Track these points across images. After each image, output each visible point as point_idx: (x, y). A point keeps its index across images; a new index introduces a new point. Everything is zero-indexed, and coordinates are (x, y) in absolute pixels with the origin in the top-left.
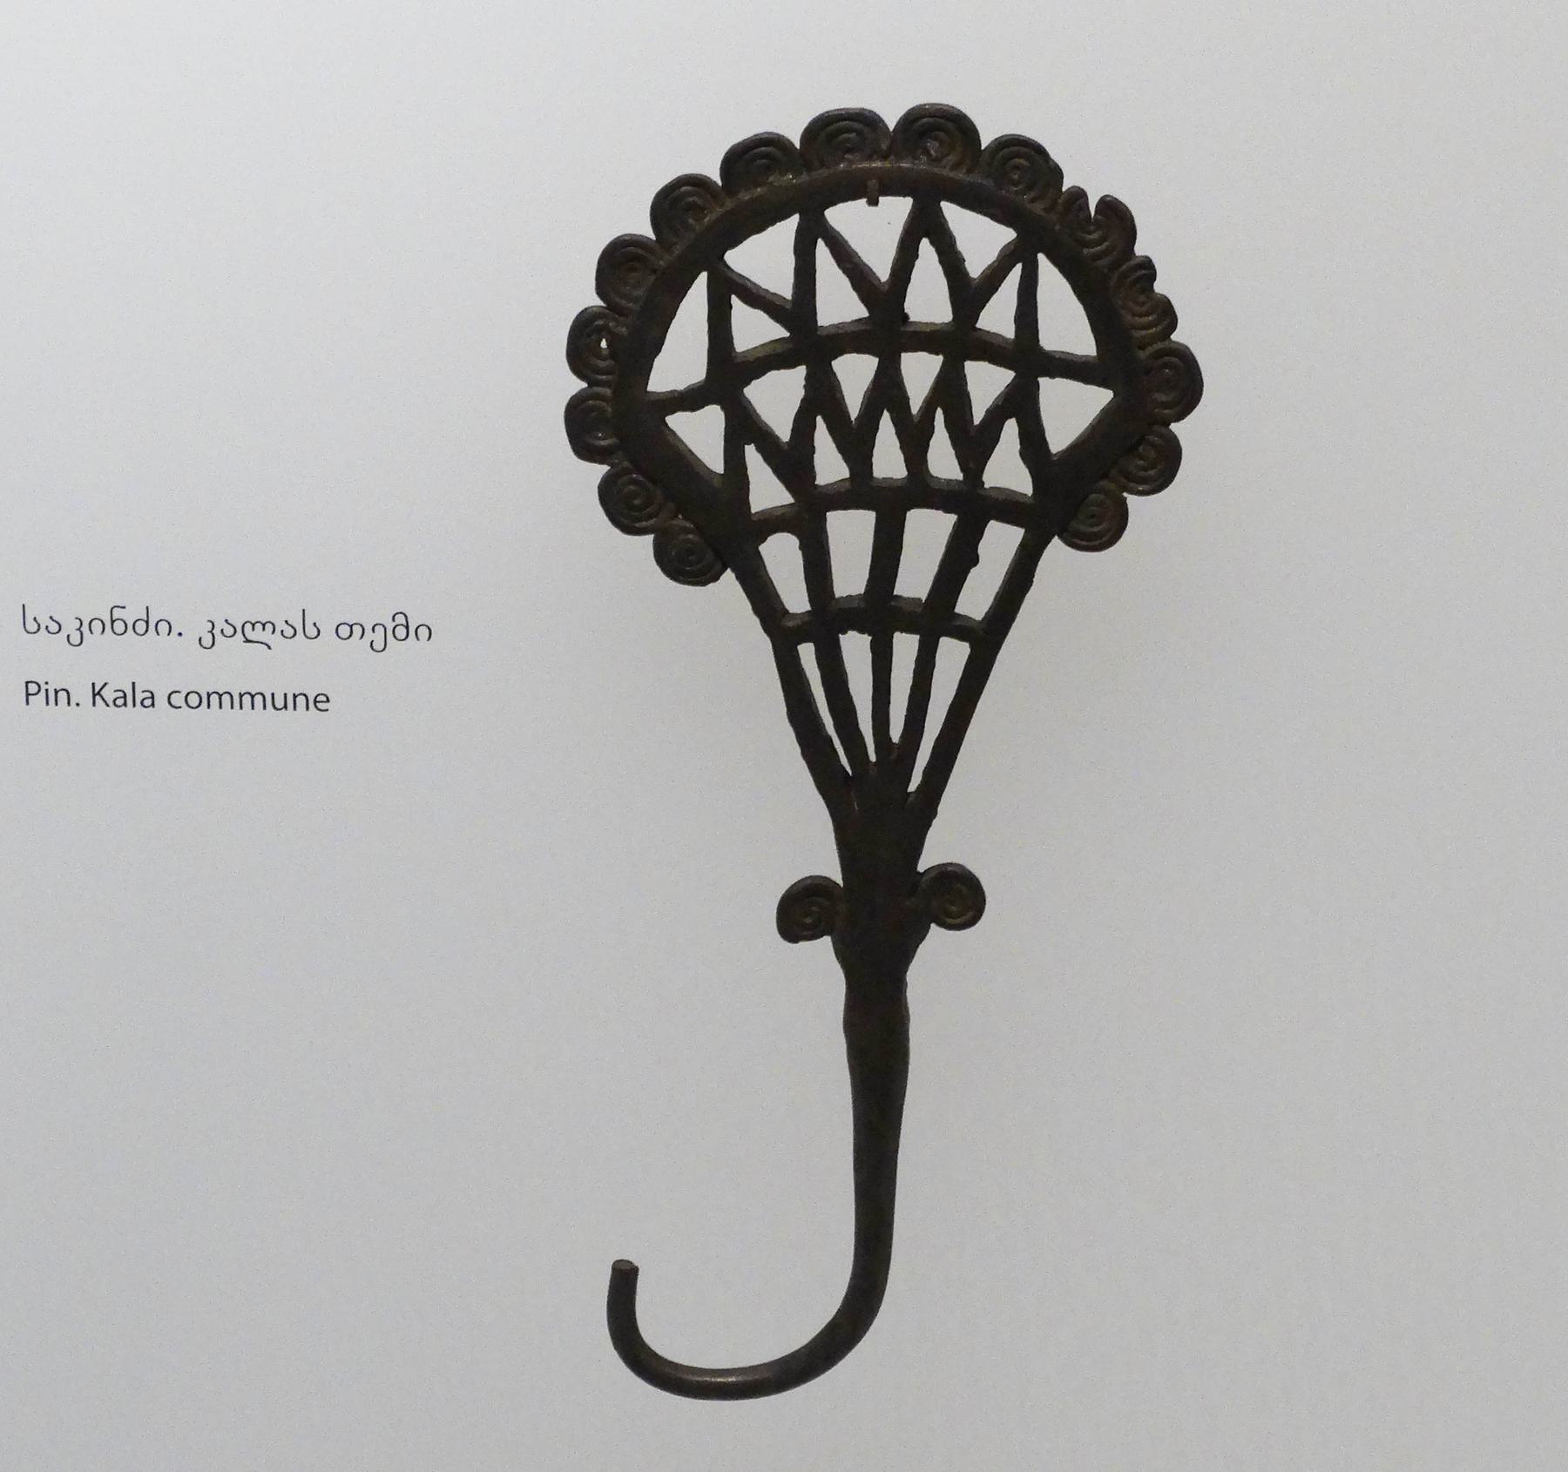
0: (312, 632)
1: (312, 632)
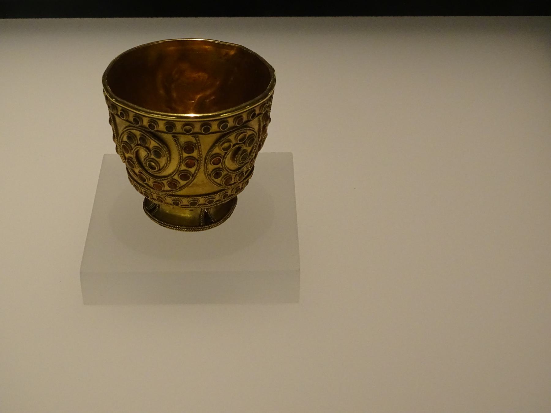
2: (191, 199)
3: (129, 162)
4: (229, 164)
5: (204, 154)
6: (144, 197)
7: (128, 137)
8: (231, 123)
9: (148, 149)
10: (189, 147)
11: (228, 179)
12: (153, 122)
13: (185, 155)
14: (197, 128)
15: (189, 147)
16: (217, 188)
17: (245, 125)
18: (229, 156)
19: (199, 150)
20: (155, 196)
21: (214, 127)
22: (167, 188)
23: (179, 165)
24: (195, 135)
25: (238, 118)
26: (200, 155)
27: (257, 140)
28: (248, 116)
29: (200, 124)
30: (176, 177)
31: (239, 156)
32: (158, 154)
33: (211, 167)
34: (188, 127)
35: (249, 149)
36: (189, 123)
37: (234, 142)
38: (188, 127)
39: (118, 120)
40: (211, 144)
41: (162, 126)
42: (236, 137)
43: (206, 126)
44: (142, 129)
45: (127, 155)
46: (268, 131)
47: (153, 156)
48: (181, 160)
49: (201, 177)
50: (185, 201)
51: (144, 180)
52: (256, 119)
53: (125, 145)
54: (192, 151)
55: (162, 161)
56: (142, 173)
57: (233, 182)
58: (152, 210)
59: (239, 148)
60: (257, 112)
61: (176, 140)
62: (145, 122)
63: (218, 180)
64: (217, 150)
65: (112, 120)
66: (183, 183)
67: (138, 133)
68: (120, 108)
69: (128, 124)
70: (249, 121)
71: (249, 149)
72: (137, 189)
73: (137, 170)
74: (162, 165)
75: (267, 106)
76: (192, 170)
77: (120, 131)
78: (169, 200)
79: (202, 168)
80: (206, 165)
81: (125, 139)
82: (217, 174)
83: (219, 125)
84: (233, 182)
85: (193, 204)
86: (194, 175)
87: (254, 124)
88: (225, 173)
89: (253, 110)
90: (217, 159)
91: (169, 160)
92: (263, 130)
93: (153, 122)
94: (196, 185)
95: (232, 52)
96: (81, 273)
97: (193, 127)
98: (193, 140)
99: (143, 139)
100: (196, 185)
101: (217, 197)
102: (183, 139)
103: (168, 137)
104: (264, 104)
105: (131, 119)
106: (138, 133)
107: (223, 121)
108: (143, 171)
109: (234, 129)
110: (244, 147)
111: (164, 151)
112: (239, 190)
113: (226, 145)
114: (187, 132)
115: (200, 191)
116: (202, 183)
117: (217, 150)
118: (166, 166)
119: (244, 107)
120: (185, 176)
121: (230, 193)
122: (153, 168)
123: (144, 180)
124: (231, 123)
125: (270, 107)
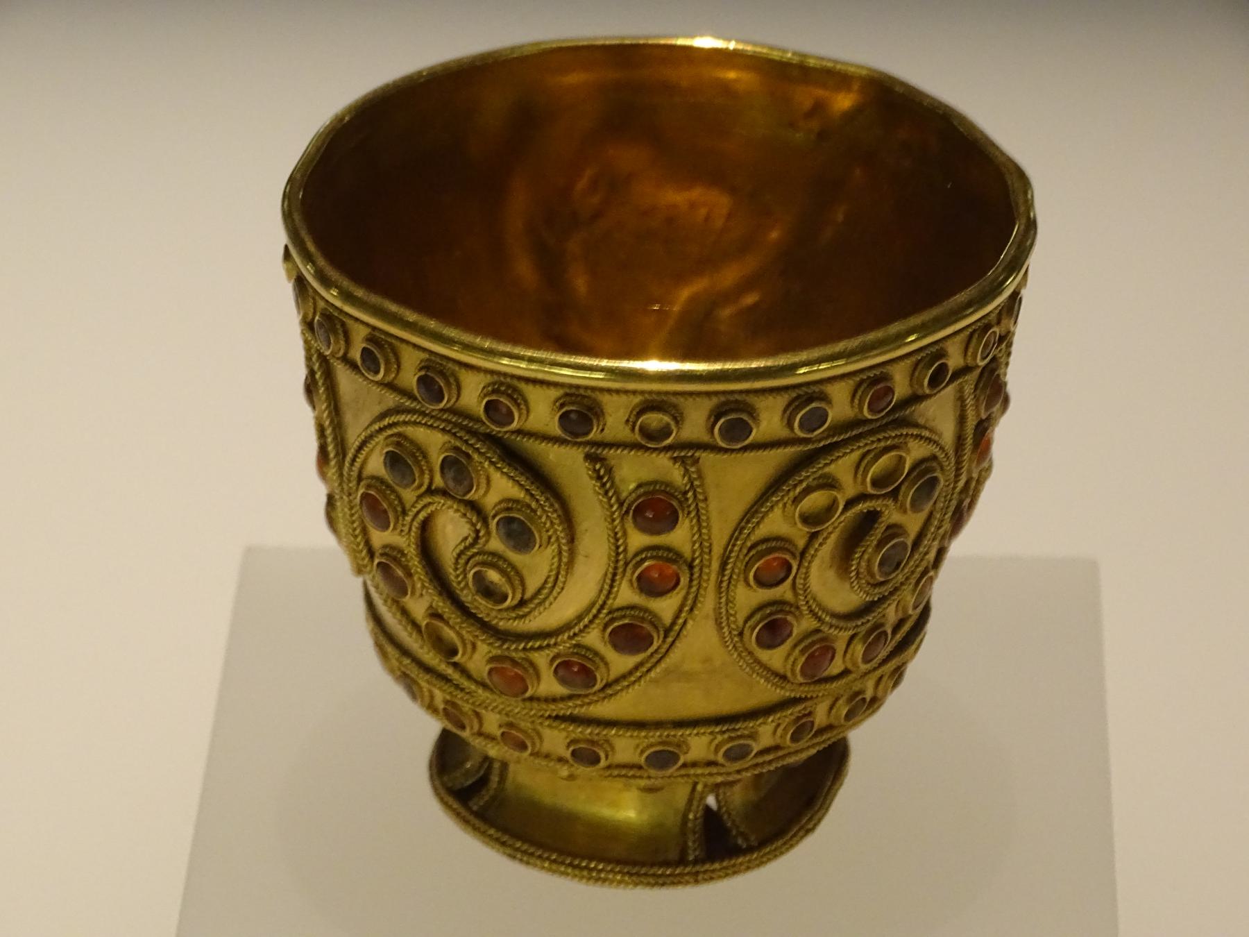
2: (655, 735)
3: (385, 568)
4: (828, 587)
5: (719, 535)
7: (393, 460)
8: (840, 406)
9: (474, 506)
10: (656, 508)
11: (818, 651)
12: (506, 393)
13: (637, 540)
14: (695, 425)
16: (766, 692)
19: (700, 521)
20: (492, 723)
21: (769, 420)
22: (549, 685)
23: (612, 580)
24: (687, 452)
25: (874, 384)
26: (704, 545)
27: (949, 486)
29: (708, 405)
30: (594, 638)
31: (869, 555)
33: (747, 597)
34: (655, 419)
36: (659, 402)
37: (850, 489)
38: (655, 419)
39: (345, 379)
40: (750, 495)
41: (542, 412)
44: (458, 422)
45: (380, 538)
47: (496, 544)
48: (619, 562)
49: (701, 640)
50: (626, 748)
52: (949, 392)
53: (367, 495)
55: (536, 565)
56: (433, 605)
57: (836, 667)
58: (469, 785)
59: (872, 517)
60: (954, 360)
62: (472, 395)
63: (775, 658)
65: (320, 384)
66: (621, 663)
67: (434, 442)
69: (391, 399)
70: (915, 399)
74: (532, 584)
75: (995, 339)
76: (665, 607)
78: (556, 739)
79: (708, 602)
81: (376, 464)
84: (836, 667)
85: (663, 759)
86: (673, 632)
87: (940, 413)
90: (777, 562)
92: (976, 440)
93: (506, 393)
95: (844, 102)
97: (678, 419)
98: (676, 475)
99: (456, 465)
101: (766, 733)
102: (633, 471)
103: (566, 462)
104: (984, 327)
105: (410, 377)
106: (434, 442)
109: (852, 430)
110: (892, 514)
111: (547, 520)
113: (816, 500)
114: (651, 439)
115: (697, 703)
116: (704, 667)
117: (776, 522)
118: (554, 584)
122: (488, 592)
124: (840, 406)
125: (1005, 339)
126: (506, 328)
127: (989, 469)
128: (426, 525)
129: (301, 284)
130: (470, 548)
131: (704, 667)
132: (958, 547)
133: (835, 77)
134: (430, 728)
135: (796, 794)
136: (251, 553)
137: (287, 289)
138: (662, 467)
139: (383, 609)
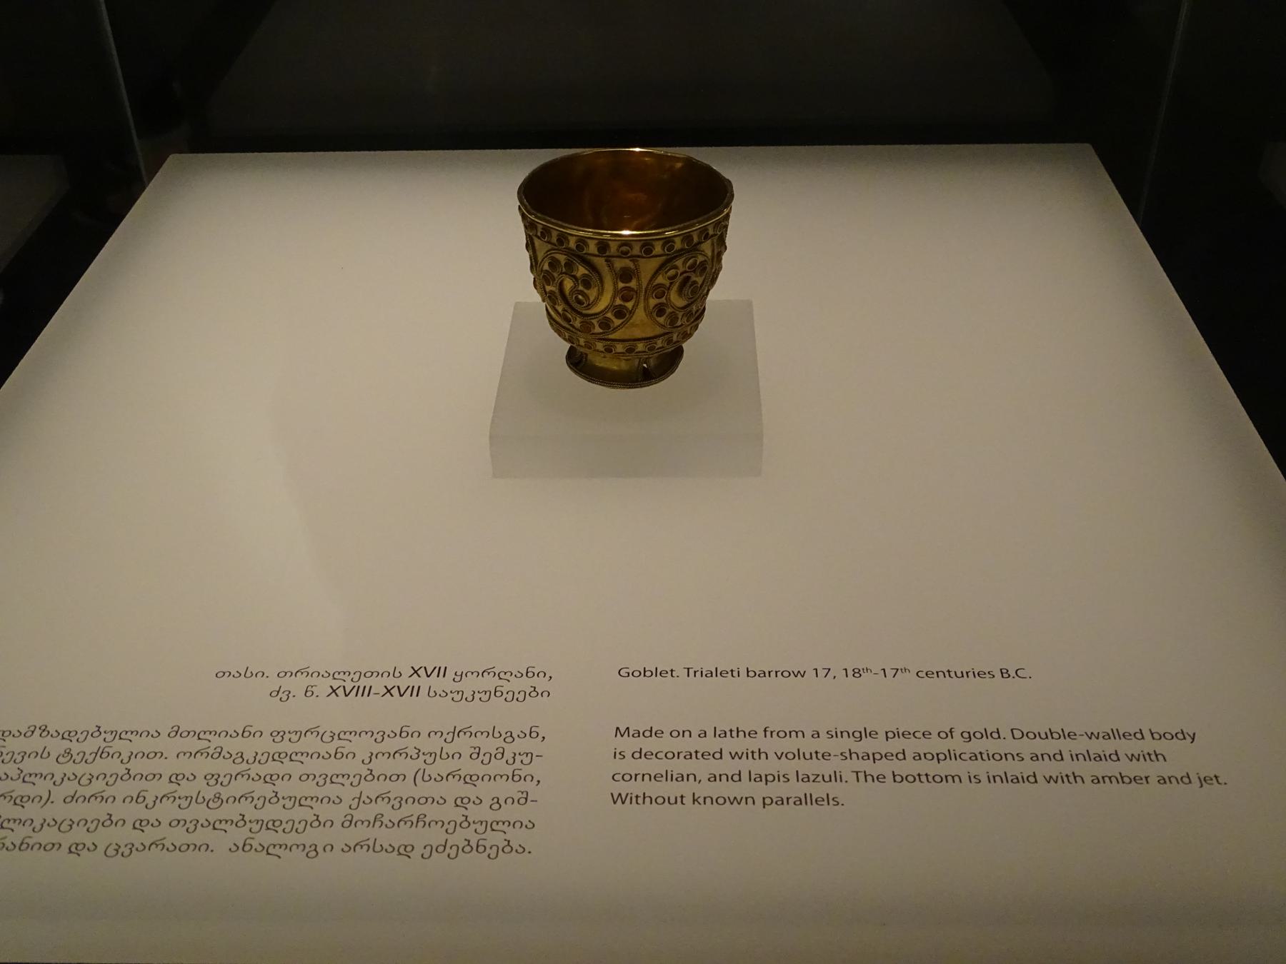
0: (397, 674)
1: (397, 674)
2: (627, 344)
3: (549, 297)
4: (677, 300)
5: (644, 283)
6: (568, 346)
7: (550, 264)
8: (678, 245)
9: (574, 277)
10: (626, 275)
11: (673, 318)
12: (582, 242)
13: (621, 285)
14: (636, 250)
15: (626, 275)
16: (659, 331)
17: (693, 248)
18: (675, 288)
19: (639, 279)
20: (582, 341)
21: (658, 249)
22: (598, 330)
23: (614, 298)
24: (634, 258)
25: (687, 238)
26: (640, 285)
27: (710, 271)
28: (699, 237)
29: (640, 244)
30: (609, 315)
31: (688, 290)
32: (587, 284)
33: (653, 302)
34: (624, 248)
35: (700, 280)
36: (626, 242)
37: (681, 269)
38: (624, 248)
39: (537, 242)
40: (652, 272)
41: (592, 248)
42: (685, 263)
43: (647, 247)
44: (569, 252)
45: (548, 288)
46: (723, 261)
47: (581, 288)
48: (616, 292)
49: (640, 314)
50: (620, 348)
51: (568, 320)
52: (709, 242)
53: (544, 276)
54: (630, 280)
55: (592, 293)
56: (566, 310)
57: (679, 323)
58: (577, 362)
59: (688, 278)
60: (711, 232)
61: (611, 265)
62: (572, 244)
63: (661, 320)
64: (660, 279)
65: (530, 245)
66: (617, 322)
67: (562, 258)
68: (540, 227)
69: (550, 246)
70: (700, 243)
71: (700, 280)
72: (557, 331)
73: (560, 309)
74: (592, 299)
75: (722, 226)
76: (629, 305)
77: (540, 259)
78: (600, 346)
79: (641, 305)
80: (646, 299)
81: (546, 267)
82: (660, 310)
83: (663, 246)
84: (679, 323)
85: (630, 350)
86: (632, 312)
87: (707, 247)
88: (669, 310)
89: (705, 229)
90: (661, 291)
91: (601, 293)
92: (718, 257)
93: (582, 242)
94: (634, 325)
95: (679, 165)
96: (491, 437)
97: (631, 247)
98: (631, 265)
99: (569, 265)
100: (634, 325)
101: (659, 343)
102: (619, 264)
103: (600, 262)
104: (718, 223)
105: (554, 240)
106: (562, 258)
107: (668, 241)
108: (567, 308)
109: (681, 253)
110: (694, 278)
111: (595, 278)
112: (687, 336)
113: (672, 272)
114: (624, 255)
115: (638, 333)
116: (641, 324)
117: (660, 279)
118: (597, 299)
119: (693, 225)
120: (620, 313)
121: (675, 338)
122: (580, 302)
123: (568, 320)
124: (678, 245)
125: (726, 227)
126: (583, 224)
127: (721, 268)
128: (561, 284)
129: (523, 216)
130: (573, 290)
131: (641, 324)
132: (715, 295)
133: (678, 159)
134: (566, 346)
135: (669, 361)
136: (517, 305)
137: (520, 218)
138: (627, 263)
139: (552, 313)
